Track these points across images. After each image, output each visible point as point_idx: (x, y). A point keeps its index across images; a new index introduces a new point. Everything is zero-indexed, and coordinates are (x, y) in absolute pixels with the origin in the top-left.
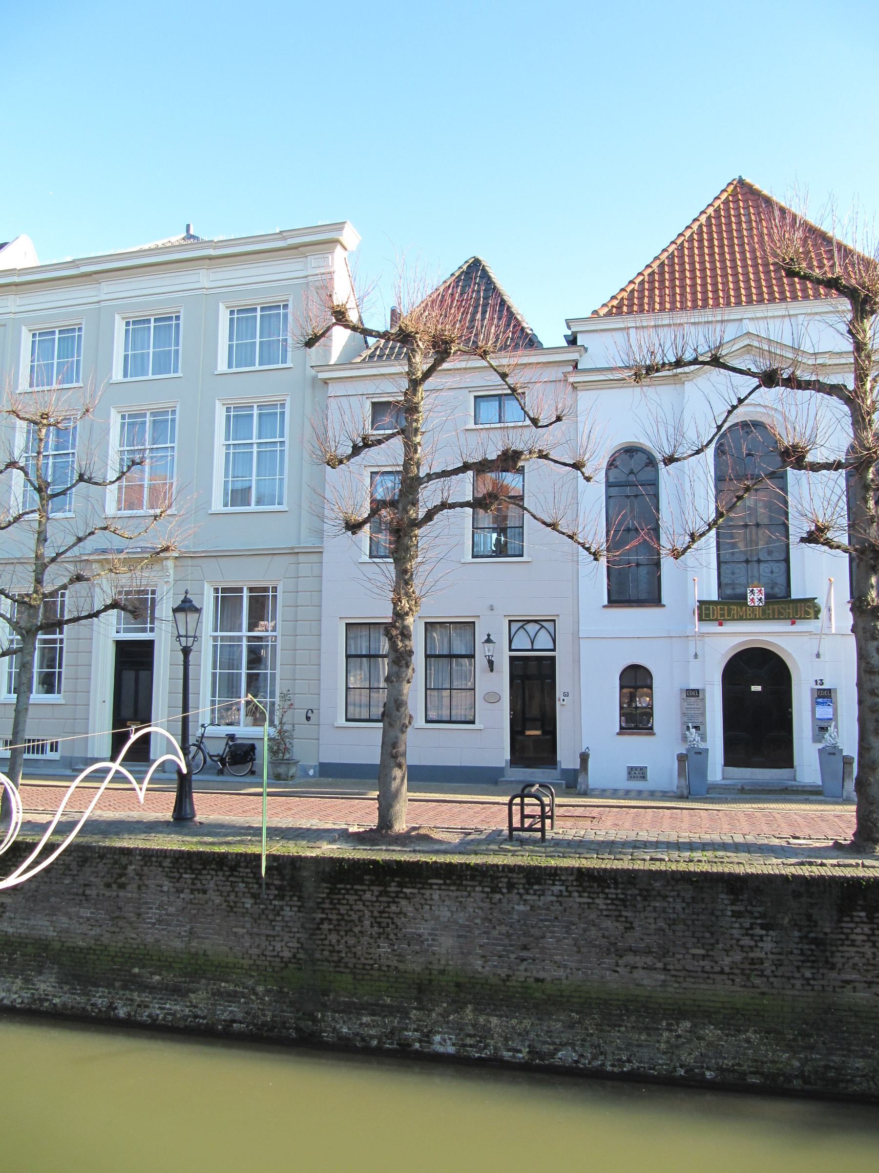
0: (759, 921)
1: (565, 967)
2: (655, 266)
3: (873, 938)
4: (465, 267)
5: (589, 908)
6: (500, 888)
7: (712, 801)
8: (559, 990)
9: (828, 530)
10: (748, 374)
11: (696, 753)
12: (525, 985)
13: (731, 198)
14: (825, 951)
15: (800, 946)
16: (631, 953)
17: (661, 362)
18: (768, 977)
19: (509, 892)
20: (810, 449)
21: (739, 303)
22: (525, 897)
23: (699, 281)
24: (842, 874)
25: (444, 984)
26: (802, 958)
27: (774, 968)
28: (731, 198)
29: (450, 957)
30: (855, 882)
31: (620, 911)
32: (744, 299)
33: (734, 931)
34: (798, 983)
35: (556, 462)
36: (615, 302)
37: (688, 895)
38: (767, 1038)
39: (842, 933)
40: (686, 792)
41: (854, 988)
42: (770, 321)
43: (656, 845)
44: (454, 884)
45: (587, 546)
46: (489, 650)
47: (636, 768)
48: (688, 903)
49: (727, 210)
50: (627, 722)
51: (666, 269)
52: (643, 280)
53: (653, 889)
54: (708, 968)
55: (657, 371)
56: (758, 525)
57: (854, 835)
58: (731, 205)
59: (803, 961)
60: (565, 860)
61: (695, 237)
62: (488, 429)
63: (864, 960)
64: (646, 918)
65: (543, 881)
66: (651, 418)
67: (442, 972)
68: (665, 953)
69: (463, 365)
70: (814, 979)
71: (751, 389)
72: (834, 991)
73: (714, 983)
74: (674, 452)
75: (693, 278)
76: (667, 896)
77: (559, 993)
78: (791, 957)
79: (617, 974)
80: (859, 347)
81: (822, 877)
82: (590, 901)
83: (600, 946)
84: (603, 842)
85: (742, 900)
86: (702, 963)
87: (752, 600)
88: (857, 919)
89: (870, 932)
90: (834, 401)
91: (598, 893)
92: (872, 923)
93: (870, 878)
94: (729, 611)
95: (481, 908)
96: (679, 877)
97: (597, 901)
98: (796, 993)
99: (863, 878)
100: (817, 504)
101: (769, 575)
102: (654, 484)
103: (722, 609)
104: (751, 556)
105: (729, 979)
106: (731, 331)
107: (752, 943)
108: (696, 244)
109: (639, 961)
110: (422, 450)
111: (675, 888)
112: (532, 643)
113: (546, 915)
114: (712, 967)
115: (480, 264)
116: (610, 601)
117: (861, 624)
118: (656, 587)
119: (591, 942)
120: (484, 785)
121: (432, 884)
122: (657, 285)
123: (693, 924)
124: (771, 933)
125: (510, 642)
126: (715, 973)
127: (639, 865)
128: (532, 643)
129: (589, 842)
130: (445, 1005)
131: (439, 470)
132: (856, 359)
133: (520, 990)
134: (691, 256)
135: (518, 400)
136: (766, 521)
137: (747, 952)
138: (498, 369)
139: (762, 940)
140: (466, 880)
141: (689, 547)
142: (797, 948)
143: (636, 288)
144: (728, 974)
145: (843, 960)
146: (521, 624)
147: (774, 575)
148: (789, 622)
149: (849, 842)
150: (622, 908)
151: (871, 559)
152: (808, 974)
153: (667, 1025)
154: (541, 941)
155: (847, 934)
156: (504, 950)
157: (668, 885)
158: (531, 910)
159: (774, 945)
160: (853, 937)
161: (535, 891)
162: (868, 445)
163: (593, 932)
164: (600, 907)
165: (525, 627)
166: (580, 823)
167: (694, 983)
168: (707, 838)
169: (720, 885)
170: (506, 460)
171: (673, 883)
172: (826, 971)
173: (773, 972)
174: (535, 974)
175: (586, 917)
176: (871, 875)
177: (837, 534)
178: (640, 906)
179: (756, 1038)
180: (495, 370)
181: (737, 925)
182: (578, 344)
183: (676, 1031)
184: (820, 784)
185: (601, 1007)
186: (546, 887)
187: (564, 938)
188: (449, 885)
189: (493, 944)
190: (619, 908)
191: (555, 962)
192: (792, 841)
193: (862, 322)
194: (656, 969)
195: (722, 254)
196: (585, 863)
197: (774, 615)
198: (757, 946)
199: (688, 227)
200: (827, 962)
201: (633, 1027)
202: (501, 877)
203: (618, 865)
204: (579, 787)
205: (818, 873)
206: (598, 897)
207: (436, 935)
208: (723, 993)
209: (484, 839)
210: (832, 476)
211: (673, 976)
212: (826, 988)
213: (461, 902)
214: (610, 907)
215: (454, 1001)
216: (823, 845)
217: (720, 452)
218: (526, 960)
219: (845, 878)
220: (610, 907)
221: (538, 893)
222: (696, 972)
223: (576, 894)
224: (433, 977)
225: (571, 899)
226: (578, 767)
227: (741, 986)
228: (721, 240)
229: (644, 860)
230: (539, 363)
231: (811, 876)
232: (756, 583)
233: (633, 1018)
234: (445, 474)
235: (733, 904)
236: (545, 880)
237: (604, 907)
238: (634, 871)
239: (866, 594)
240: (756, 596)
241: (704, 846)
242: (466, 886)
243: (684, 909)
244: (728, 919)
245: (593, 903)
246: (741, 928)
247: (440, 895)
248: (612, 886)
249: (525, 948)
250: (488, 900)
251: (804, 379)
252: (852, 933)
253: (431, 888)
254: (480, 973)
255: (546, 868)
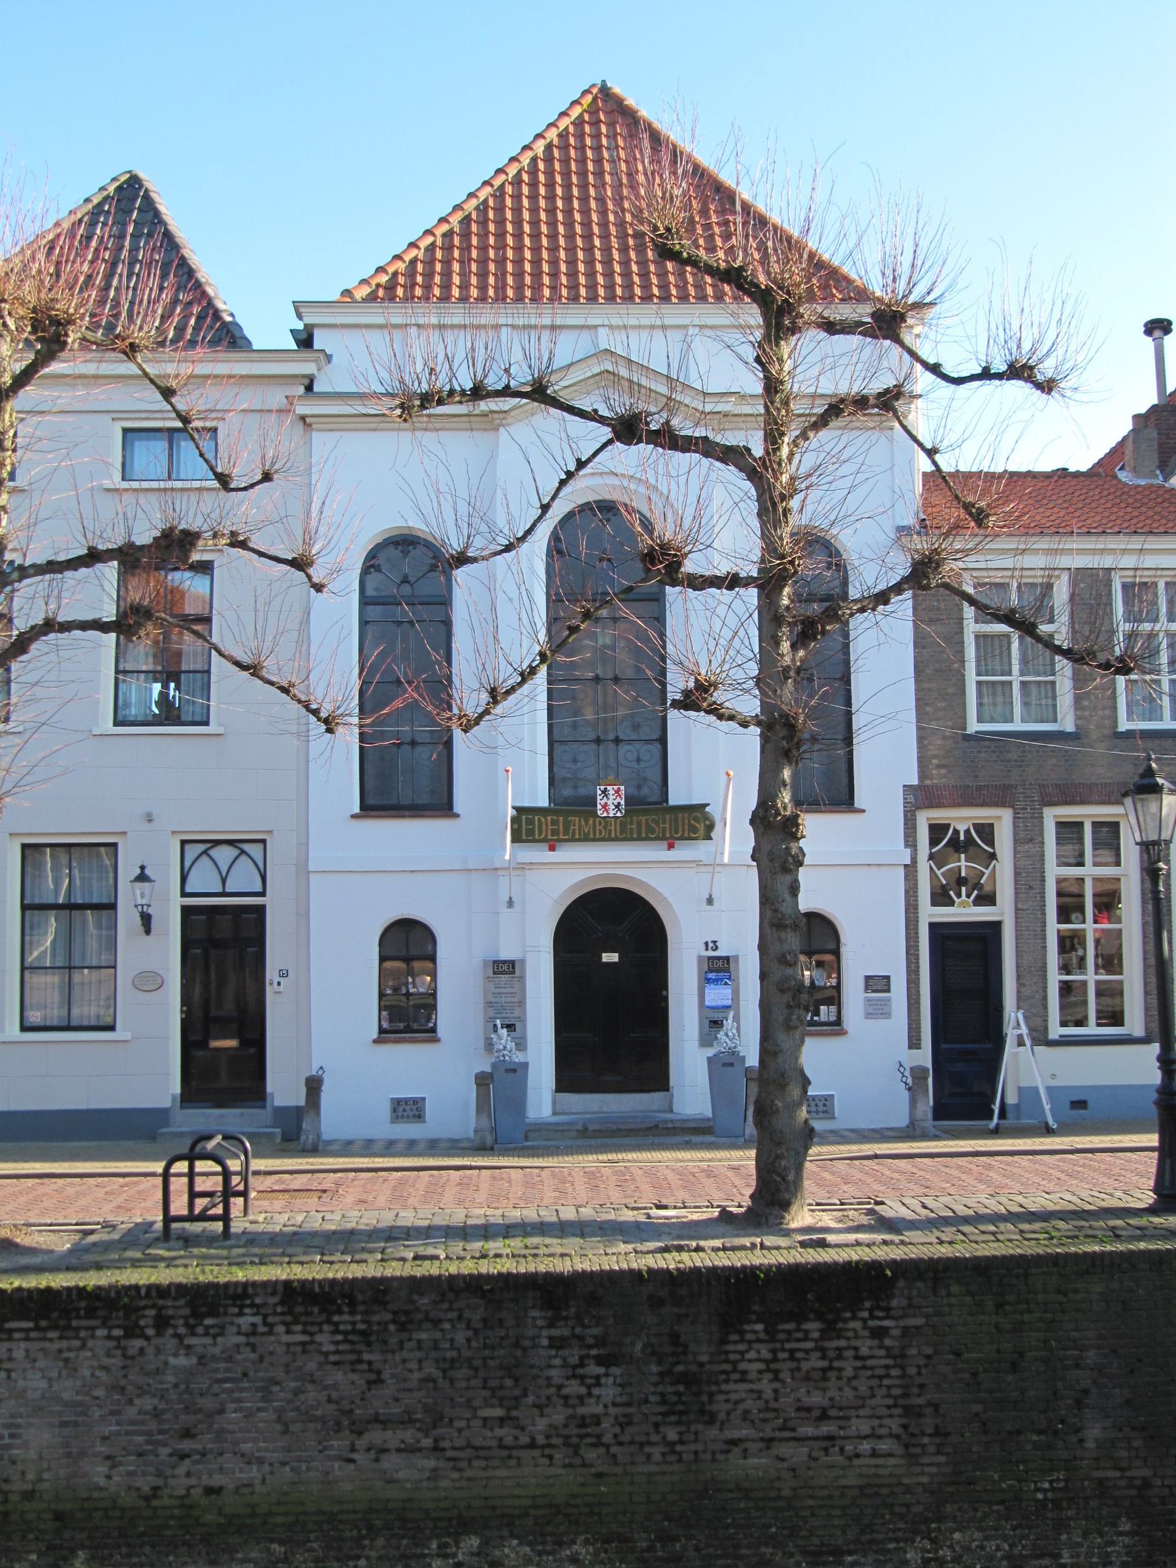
0: (594, 1352)
1: (261, 1462)
2: (455, 220)
3: (773, 1366)
4: (111, 189)
5: (304, 1352)
6: (142, 1328)
7: (533, 1152)
8: (249, 1505)
9: (716, 688)
10: (593, 419)
11: (507, 1071)
12: (187, 1502)
13: (586, 117)
14: (697, 1394)
15: (660, 1388)
16: (378, 1426)
17: (447, 388)
18: (608, 1446)
19: (159, 1334)
20: (690, 552)
21: (592, 299)
22: (187, 1341)
23: (528, 255)
24: (727, 1263)
25: (31, 1516)
26: (663, 1409)
27: (617, 1430)
28: (586, 117)
29: (45, 1465)
30: (746, 1277)
31: (359, 1353)
32: (601, 291)
33: (553, 1373)
34: (656, 1452)
35: (261, 554)
36: (384, 279)
37: (476, 1316)
38: (606, 1551)
39: (727, 1361)
40: (489, 1140)
41: (745, 1450)
42: (633, 335)
43: (427, 1233)
44: (55, 1327)
45: (314, 706)
46: (143, 895)
47: (406, 1101)
48: (476, 1331)
49: (580, 136)
50: (391, 1020)
51: (474, 228)
52: (433, 244)
53: (417, 1310)
54: (509, 1441)
55: (440, 402)
56: (616, 680)
57: (752, 1197)
58: (587, 129)
59: (664, 1414)
60: (263, 1268)
61: (525, 177)
62: (135, 490)
63: (760, 1404)
64: (404, 1361)
65: (222, 1310)
66: (429, 486)
67: (29, 1495)
68: (438, 1419)
69: (91, 369)
70: (681, 1442)
71: (599, 445)
72: (714, 1460)
73: (519, 1465)
74: (467, 548)
75: (519, 249)
76: (440, 1321)
77: (249, 1511)
78: (645, 1409)
79: (352, 1466)
80: (772, 386)
81: (696, 1270)
82: (306, 1338)
83: (322, 1419)
84: (334, 1232)
85: (566, 1319)
86: (499, 1432)
87: (605, 806)
88: (749, 1336)
89: (769, 1356)
90: (730, 474)
91: (320, 1324)
92: (772, 1340)
93: (770, 1266)
94: (567, 826)
95: (105, 1368)
96: (462, 1285)
97: (318, 1338)
98: (652, 1468)
99: (759, 1268)
100: (698, 643)
101: (635, 765)
102: (445, 602)
103: (554, 822)
104: (605, 732)
105: (543, 1456)
106: (567, 348)
107: (583, 1390)
108: (525, 190)
109: (391, 1438)
110: (10, 522)
111: (456, 1306)
112: (224, 881)
113: (227, 1370)
114: (516, 1438)
115: (141, 186)
116: (364, 806)
117: (766, 848)
118: (445, 782)
119: (307, 1413)
120: (131, 1143)
121: (12, 1331)
122: (456, 254)
123: (485, 1365)
124: (615, 1370)
125: (184, 879)
126: (522, 1447)
127: (393, 1270)
128: (224, 881)
129: (309, 1233)
130: (34, 1557)
131: (41, 560)
132: (766, 407)
133: (176, 1512)
134: (517, 210)
135: (193, 439)
136: (630, 673)
137: (574, 1407)
138: (156, 380)
139: (598, 1384)
140: (78, 1317)
141: (487, 712)
142: (654, 1393)
143: (421, 256)
144: (543, 1447)
145: (729, 1406)
146: (202, 847)
147: (642, 765)
148: (665, 844)
149: (743, 1210)
150: (363, 1347)
151: (783, 738)
152: (672, 1435)
153: (439, 1547)
154: (217, 1418)
155: (734, 1363)
156: (148, 1442)
157: (442, 1301)
158: (199, 1363)
159: (619, 1390)
160: (743, 1366)
161: (207, 1328)
162: (780, 550)
163: (312, 1395)
164: (325, 1349)
165: (213, 852)
166: (299, 1202)
167: (485, 1469)
168: (515, 1215)
169: (531, 1294)
170: (168, 547)
171: (451, 1296)
172: (700, 1427)
173: (616, 1436)
174: (206, 1481)
175: (300, 1368)
176: (773, 1261)
177: (730, 696)
178: (393, 1341)
179: (588, 1553)
180: (152, 381)
181: (557, 1362)
182: (315, 347)
183: (455, 1555)
184: (710, 1115)
185: (325, 1527)
186: (228, 1319)
187: (259, 1410)
188: (45, 1330)
189: (127, 1433)
190: (358, 1347)
191: (243, 1455)
192: (655, 1212)
193: (777, 345)
194: (420, 1450)
195: (568, 212)
196: (299, 1273)
197: (639, 833)
198: (590, 1395)
199: (513, 159)
200: (702, 1412)
201: (380, 1558)
202: (145, 1307)
203: (356, 1271)
204: (303, 1137)
205: (690, 1264)
206: (321, 1331)
207: (18, 1426)
208: (533, 1481)
209: (119, 1241)
210: (722, 599)
211: (450, 1459)
212: (702, 1456)
213: (67, 1360)
214: (341, 1347)
215: (51, 1548)
216: (705, 1216)
217: (556, 549)
218: (188, 1456)
219: (733, 1269)
220: (341, 1347)
221: (212, 1331)
222: (490, 1448)
223: (281, 1329)
224: (10, 1507)
225: (272, 1338)
226: (302, 1102)
227: (565, 1466)
228: (567, 186)
229: (404, 1260)
230: (231, 377)
231: (678, 1269)
232: (611, 778)
233: (380, 1542)
234: (52, 567)
235: (551, 1325)
236: (226, 1306)
237: (332, 1348)
238: (383, 1280)
239: (774, 797)
240: (612, 801)
241: (508, 1230)
242: (78, 1329)
243: (469, 1340)
244: (542, 1352)
245: (312, 1342)
246: (565, 1365)
247: (27, 1351)
248: (346, 1309)
249: (187, 1434)
250: (119, 1352)
251: (683, 433)
252: (743, 1360)
253: (10, 1339)
254: (101, 1489)
255: (227, 1285)
